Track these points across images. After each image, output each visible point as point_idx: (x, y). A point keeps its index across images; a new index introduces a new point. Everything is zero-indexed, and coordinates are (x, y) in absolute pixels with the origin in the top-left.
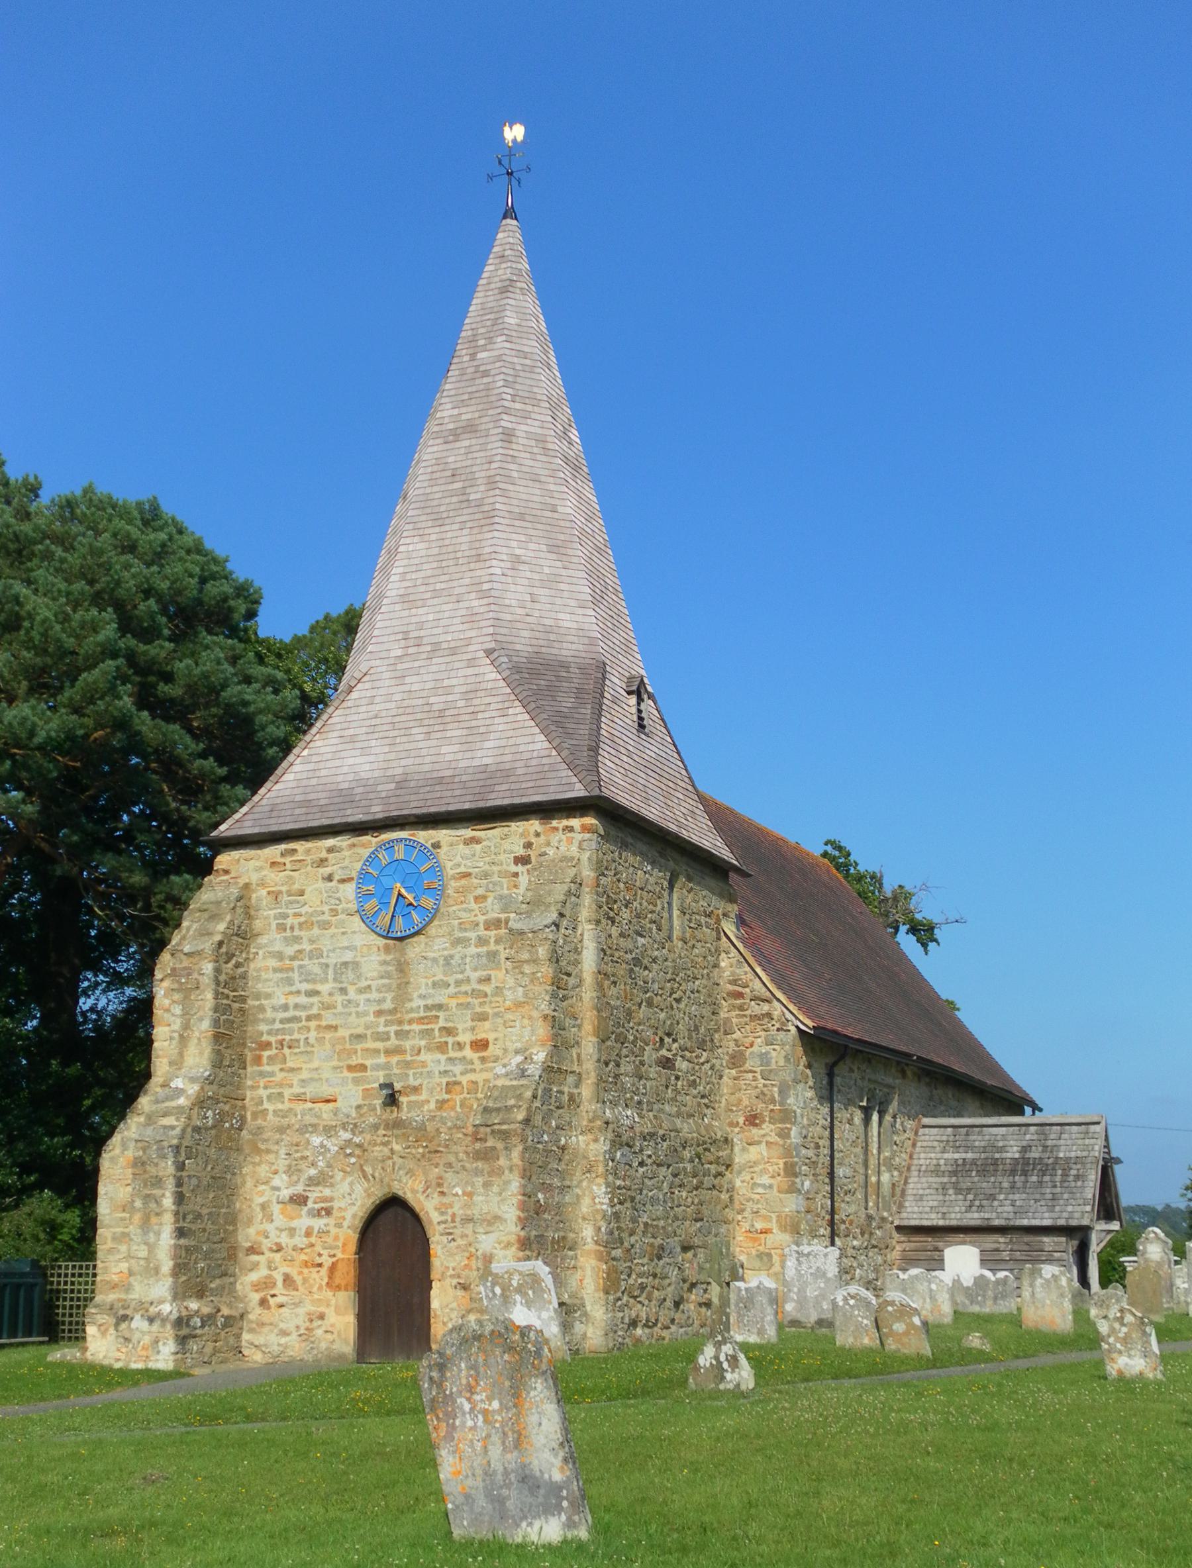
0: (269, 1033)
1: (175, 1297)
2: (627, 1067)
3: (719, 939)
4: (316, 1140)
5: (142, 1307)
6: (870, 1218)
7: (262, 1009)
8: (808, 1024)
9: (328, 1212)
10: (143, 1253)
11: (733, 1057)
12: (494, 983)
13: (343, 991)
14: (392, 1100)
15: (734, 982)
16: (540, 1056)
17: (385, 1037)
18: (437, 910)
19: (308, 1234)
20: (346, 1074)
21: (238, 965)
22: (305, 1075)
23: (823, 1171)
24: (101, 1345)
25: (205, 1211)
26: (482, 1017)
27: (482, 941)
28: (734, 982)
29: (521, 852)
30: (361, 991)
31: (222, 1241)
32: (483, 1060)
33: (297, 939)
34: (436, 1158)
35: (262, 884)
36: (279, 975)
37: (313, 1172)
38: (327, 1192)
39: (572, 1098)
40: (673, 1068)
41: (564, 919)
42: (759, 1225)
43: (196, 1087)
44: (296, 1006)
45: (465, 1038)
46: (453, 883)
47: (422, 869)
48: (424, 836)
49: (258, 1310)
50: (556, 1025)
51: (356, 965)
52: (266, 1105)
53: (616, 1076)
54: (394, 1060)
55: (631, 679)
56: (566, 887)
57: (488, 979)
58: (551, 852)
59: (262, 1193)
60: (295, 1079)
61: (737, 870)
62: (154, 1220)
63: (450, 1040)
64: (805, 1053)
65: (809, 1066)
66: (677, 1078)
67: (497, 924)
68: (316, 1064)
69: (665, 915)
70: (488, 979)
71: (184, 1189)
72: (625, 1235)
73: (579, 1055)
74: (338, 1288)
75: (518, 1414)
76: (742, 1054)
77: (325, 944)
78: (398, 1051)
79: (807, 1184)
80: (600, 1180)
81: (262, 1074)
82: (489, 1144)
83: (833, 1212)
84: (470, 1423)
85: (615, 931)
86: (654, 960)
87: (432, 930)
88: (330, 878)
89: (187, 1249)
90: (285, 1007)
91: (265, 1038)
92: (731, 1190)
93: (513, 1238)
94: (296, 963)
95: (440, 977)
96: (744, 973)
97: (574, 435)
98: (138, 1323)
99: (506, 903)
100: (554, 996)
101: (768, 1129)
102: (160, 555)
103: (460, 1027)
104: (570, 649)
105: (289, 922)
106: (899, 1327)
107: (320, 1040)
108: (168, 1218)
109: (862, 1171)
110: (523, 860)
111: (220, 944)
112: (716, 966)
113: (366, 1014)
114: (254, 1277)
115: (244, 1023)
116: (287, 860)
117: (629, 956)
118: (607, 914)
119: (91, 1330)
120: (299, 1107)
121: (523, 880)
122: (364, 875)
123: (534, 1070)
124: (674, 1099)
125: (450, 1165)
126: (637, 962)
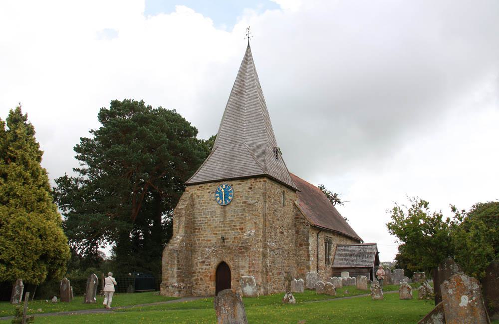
4: (207, 249)
9: (210, 265)
13: (212, 217)
15: (297, 215)
17: (220, 227)
19: (205, 269)
21: (190, 211)
25: (184, 264)
26: (242, 223)
27: (242, 206)
29: (250, 187)
30: (216, 217)
33: (203, 206)
37: (206, 256)
38: (209, 260)
43: (182, 238)
45: (238, 227)
55: (275, 148)
57: (243, 215)
61: (298, 191)
78: (224, 230)
82: (243, 250)
88: (209, 192)
90: (200, 220)
105: (201, 202)
107: (208, 228)
108: (176, 265)
113: (217, 222)
114: (194, 278)
119: (161, 289)
125: (235, 255)
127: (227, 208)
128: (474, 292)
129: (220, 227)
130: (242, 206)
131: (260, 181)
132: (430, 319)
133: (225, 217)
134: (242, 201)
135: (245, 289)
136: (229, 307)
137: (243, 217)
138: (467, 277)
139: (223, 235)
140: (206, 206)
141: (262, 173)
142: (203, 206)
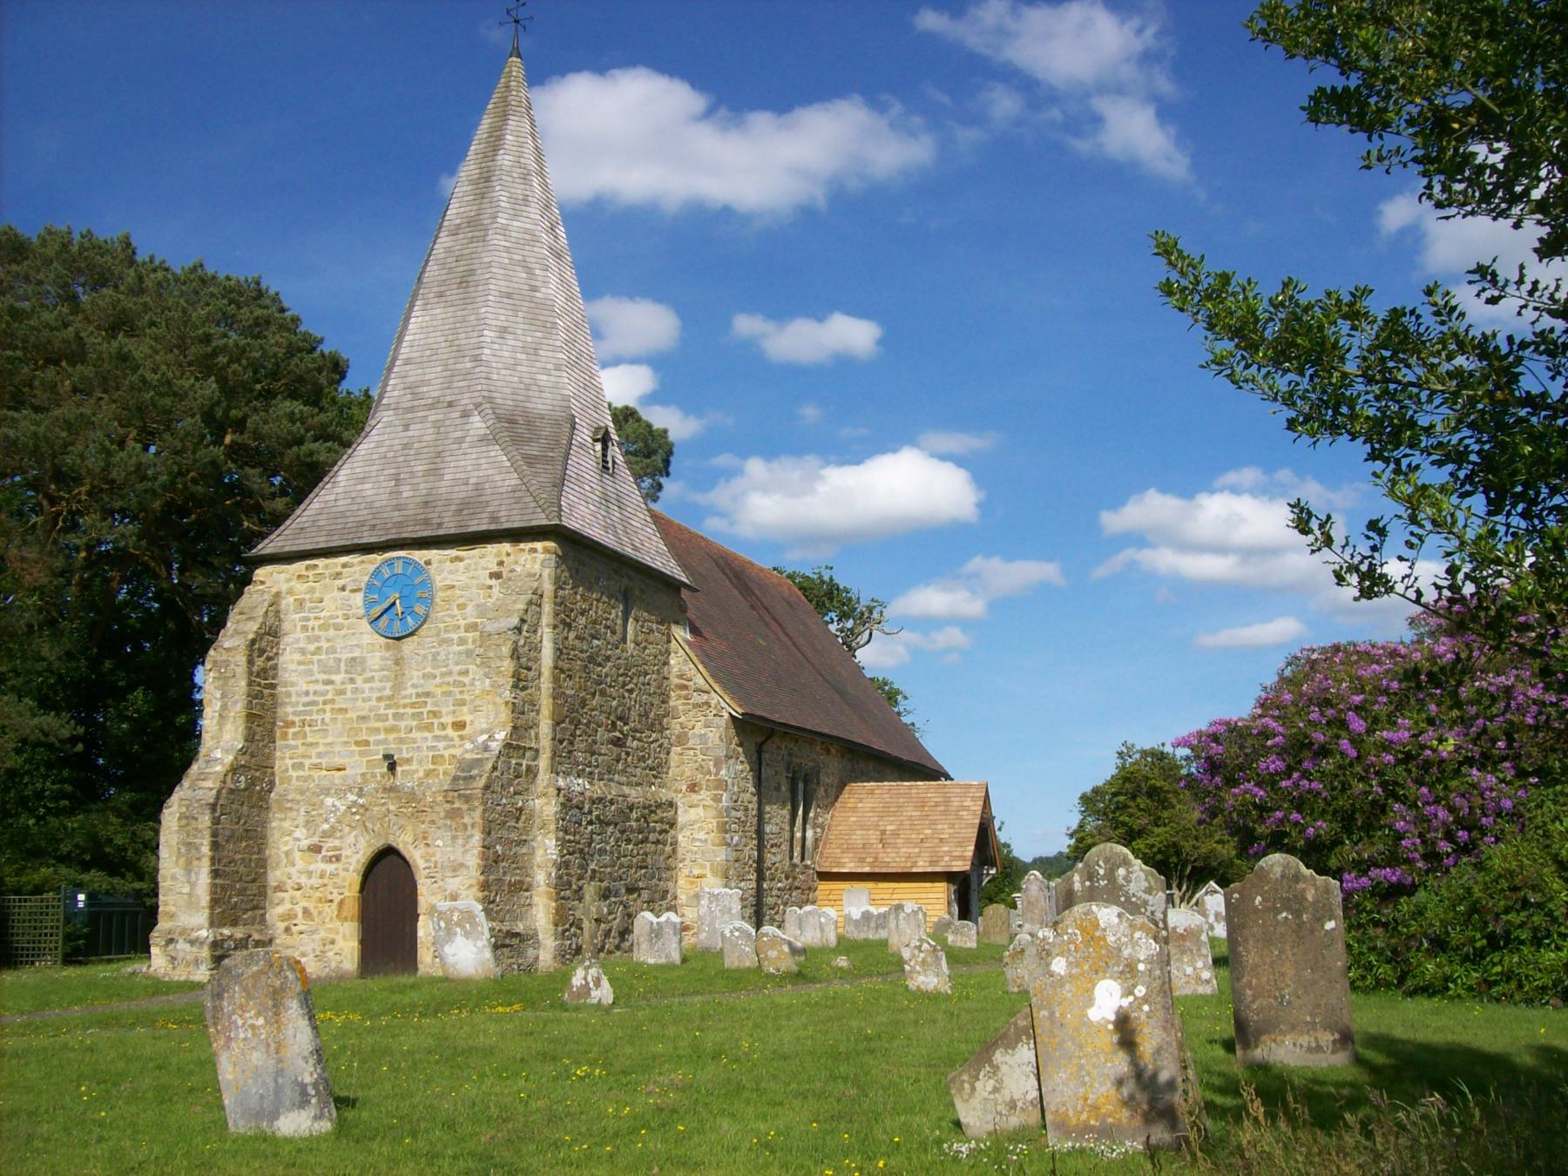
0: (294, 713)
1: (212, 924)
2: (580, 744)
3: (669, 641)
4: (329, 801)
5: (184, 931)
6: (795, 866)
7: (289, 695)
8: (738, 711)
9: (338, 859)
10: (186, 890)
11: (678, 737)
12: (471, 676)
13: (352, 681)
14: (392, 767)
15: (681, 677)
16: (501, 735)
17: (379, 718)
18: (427, 616)
19: (322, 876)
20: (354, 748)
22: (321, 749)
23: (751, 829)
24: (158, 960)
26: (462, 703)
27: (462, 641)
28: (681, 677)
29: (495, 569)
30: (366, 681)
31: (254, 881)
32: (462, 738)
33: (318, 639)
34: (422, 817)
35: (290, 592)
36: (302, 667)
37: (326, 826)
38: (337, 843)
39: (529, 768)
40: (623, 745)
41: (526, 626)
42: (696, 872)
43: (231, 758)
44: (315, 693)
45: (449, 720)
46: (441, 594)
47: (416, 581)
48: (419, 555)
49: (284, 936)
50: (517, 710)
51: (363, 661)
52: (291, 772)
53: (570, 752)
54: (391, 737)
55: (599, 428)
56: (529, 596)
57: (466, 672)
58: (519, 569)
59: (286, 843)
60: (313, 752)
62: (195, 863)
63: (436, 721)
64: (738, 734)
65: (740, 745)
66: (628, 754)
67: (472, 627)
68: (329, 740)
69: (619, 621)
70: (466, 672)
71: (220, 839)
72: (574, 880)
73: (537, 734)
74: (346, 919)
75: (279, 1029)
76: (686, 734)
77: (339, 645)
79: (736, 839)
80: (552, 836)
81: (287, 746)
82: (456, 805)
83: (760, 860)
84: (242, 1035)
85: (572, 635)
86: (608, 659)
87: (422, 632)
88: (343, 589)
89: (222, 887)
90: (307, 693)
91: (291, 718)
92: (675, 843)
93: (474, 882)
94: (316, 658)
95: (429, 670)
96: (689, 669)
97: (561, 231)
98: (182, 945)
99: (482, 610)
100: (515, 686)
101: (704, 795)
102: (258, 327)
103: (444, 710)
104: (542, 404)
105: (310, 624)
106: (773, 954)
107: (334, 720)
108: (206, 862)
109: (787, 828)
110: (496, 576)
111: (253, 642)
112: (666, 663)
113: (369, 699)
114: (280, 910)
115: (275, 705)
116: (311, 573)
117: (585, 655)
118: (564, 622)
119: (154, 950)
120: (316, 774)
121: (495, 590)
122: (370, 587)
123: (496, 746)
124: (624, 771)
125: (433, 822)
126: (591, 659)
127: (408, 646)
128: (1141, 967)
129: (379, 718)
130: (462, 641)
131: (534, 550)
132: (992, 1066)
133: (398, 687)
134: (462, 623)
135: (448, 950)
136: (258, 1014)
137: (466, 680)
138: (1119, 915)
139: (392, 748)
140: (328, 641)
141: (541, 520)
142: (318, 639)
